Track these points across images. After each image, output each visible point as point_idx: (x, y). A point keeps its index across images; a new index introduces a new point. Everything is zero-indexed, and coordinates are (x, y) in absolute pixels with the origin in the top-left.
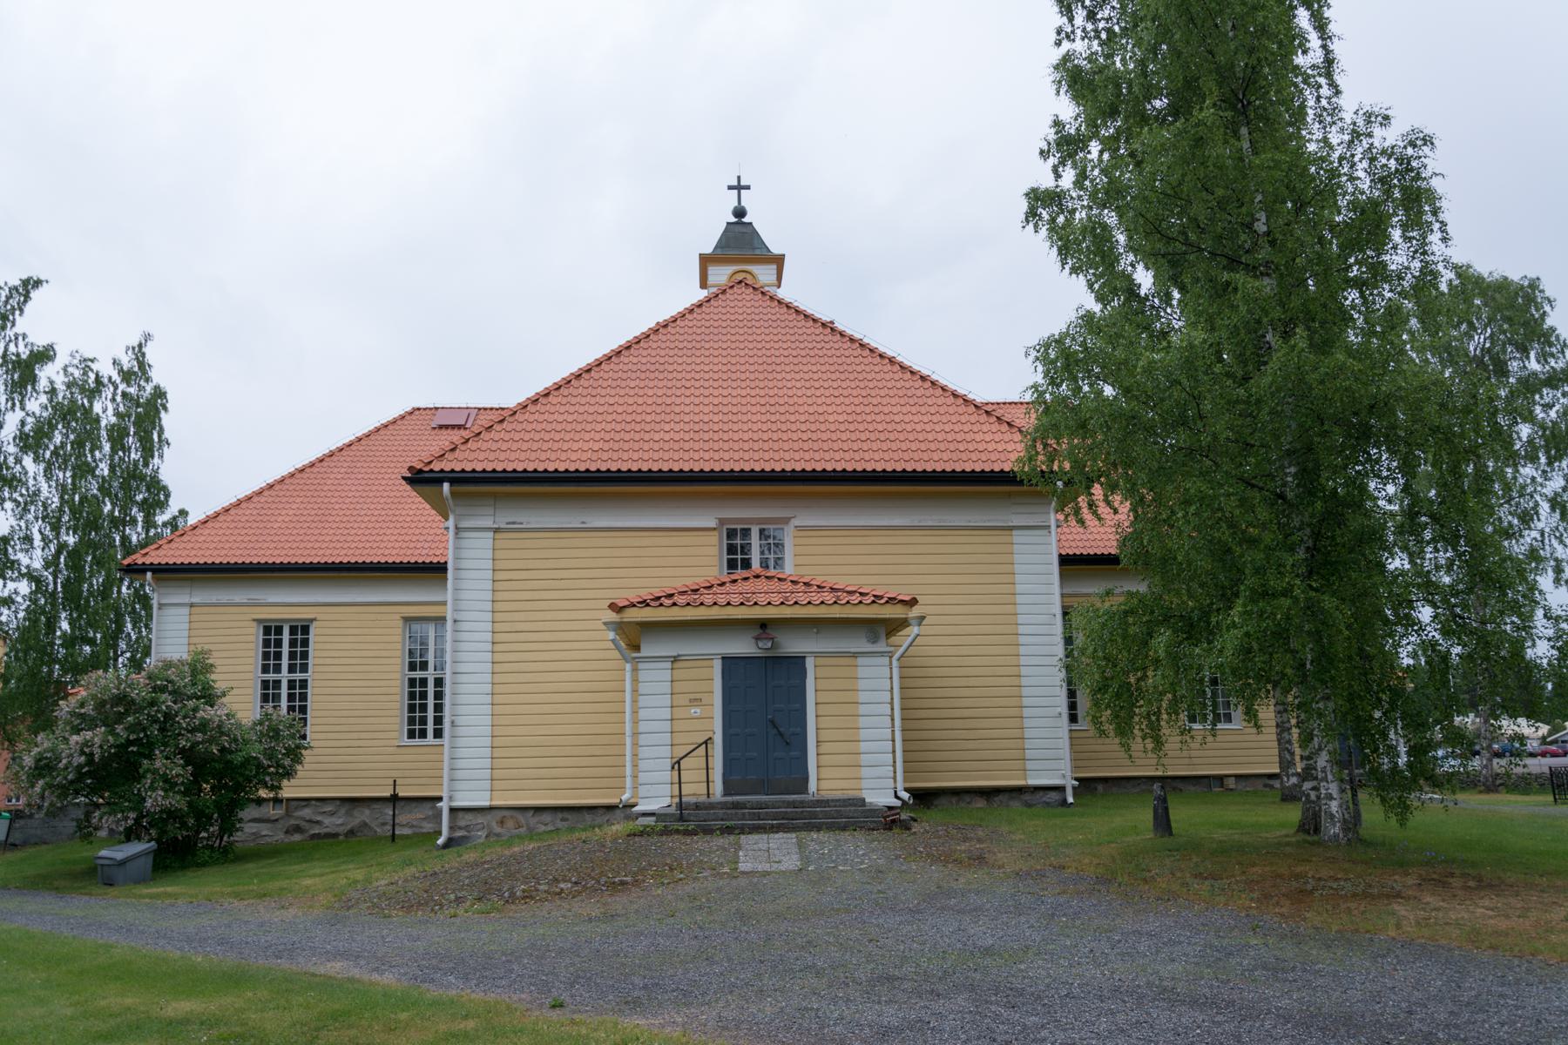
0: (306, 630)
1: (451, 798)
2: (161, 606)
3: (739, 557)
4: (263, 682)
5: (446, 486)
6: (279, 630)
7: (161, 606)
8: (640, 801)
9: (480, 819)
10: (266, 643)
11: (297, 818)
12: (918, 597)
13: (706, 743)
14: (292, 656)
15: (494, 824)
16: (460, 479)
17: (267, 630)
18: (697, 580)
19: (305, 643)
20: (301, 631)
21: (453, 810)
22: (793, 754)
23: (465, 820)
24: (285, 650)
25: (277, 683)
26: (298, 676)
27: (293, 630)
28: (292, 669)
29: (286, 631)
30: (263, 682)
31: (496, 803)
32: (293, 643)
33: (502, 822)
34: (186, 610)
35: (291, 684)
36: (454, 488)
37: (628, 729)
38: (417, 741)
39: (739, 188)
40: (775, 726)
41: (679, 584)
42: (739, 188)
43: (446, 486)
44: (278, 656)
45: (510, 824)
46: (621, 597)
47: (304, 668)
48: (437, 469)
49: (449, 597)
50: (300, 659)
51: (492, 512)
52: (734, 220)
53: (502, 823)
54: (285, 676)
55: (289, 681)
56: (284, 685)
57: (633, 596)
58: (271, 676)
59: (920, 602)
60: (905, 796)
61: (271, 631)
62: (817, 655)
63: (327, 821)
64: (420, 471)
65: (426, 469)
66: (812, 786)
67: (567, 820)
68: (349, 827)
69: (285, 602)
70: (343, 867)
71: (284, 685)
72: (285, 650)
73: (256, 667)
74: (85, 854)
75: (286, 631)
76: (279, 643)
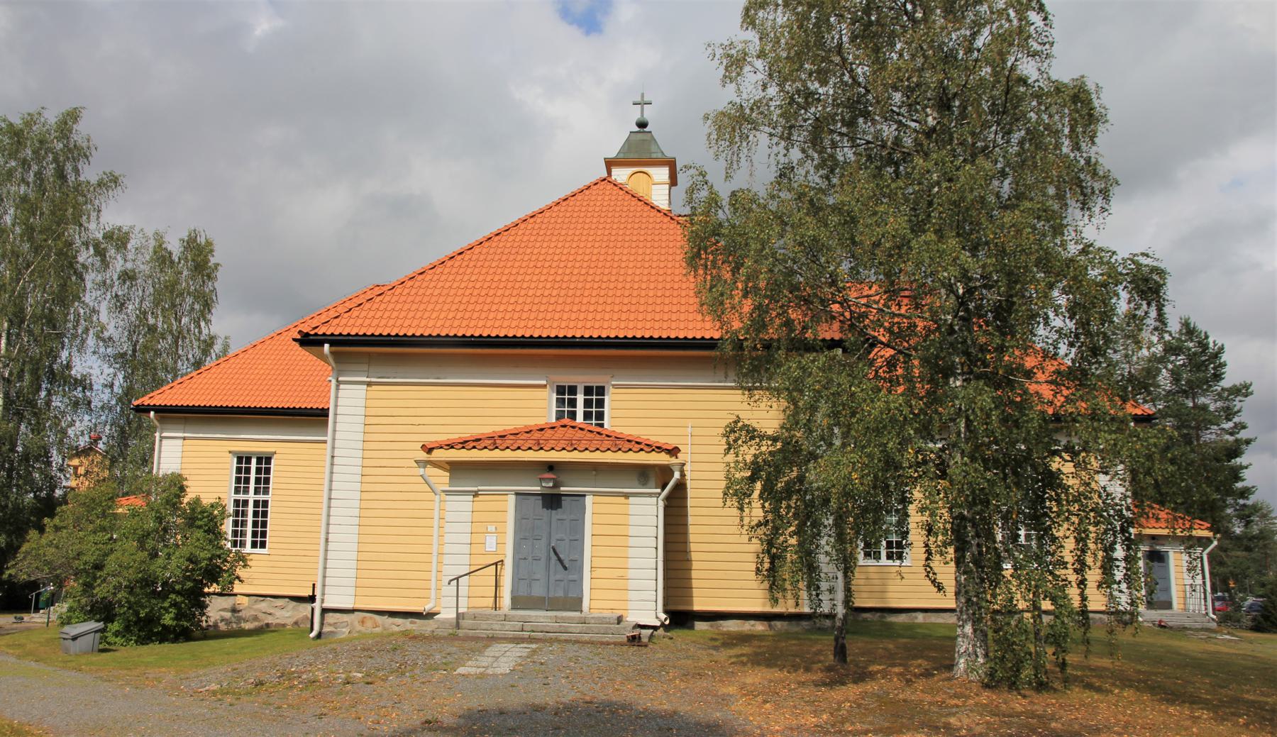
0: (268, 460)
1: (323, 601)
2: (162, 438)
3: (594, 410)
4: (235, 501)
5: (327, 346)
6: (248, 460)
7: (162, 438)
8: (442, 611)
9: (345, 617)
10: (239, 470)
11: (256, 610)
12: (680, 447)
13: (496, 564)
14: (258, 481)
15: (356, 623)
16: (338, 341)
17: (240, 460)
18: (507, 428)
19: (268, 471)
20: (264, 460)
21: (325, 611)
22: (571, 577)
23: (330, 618)
24: (253, 476)
25: (246, 503)
26: (261, 497)
27: (259, 460)
28: (257, 491)
29: (254, 461)
30: (235, 501)
31: (358, 606)
32: (258, 471)
33: (363, 622)
34: (180, 442)
35: (256, 503)
36: (334, 349)
37: (435, 548)
38: (258, 550)
39: (642, 103)
40: (556, 553)
41: (487, 430)
42: (642, 103)
43: (327, 346)
44: (247, 480)
45: (369, 624)
46: (431, 439)
47: (266, 491)
48: (320, 333)
49: (329, 438)
50: (263, 483)
51: (366, 369)
52: (637, 129)
53: (363, 622)
54: (251, 497)
55: (255, 501)
56: (251, 504)
57: (442, 438)
58: (241, 497)
59: (683, 451)
60: (663, 616)
61: (243, 459)
62: (595, 494)
63: (278, 613)
64: (307, 334)
65: (312, 333)
66: (586, 603)
67: (415, 623)
68: (295, 620)
69: (254, 441)
70: (1205, 656)
71: (251, 504)
72: (253, 476)
73: (230, 489)
74: (1148, 640)
75: (254, 461)
76: (248, 471)
